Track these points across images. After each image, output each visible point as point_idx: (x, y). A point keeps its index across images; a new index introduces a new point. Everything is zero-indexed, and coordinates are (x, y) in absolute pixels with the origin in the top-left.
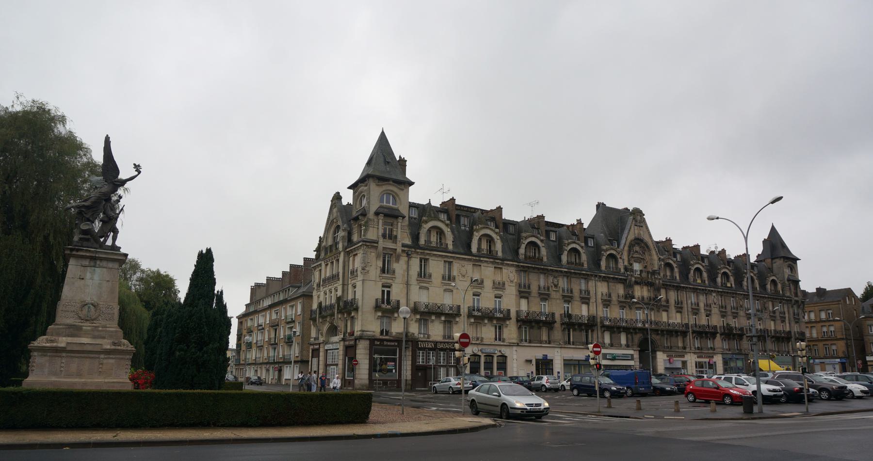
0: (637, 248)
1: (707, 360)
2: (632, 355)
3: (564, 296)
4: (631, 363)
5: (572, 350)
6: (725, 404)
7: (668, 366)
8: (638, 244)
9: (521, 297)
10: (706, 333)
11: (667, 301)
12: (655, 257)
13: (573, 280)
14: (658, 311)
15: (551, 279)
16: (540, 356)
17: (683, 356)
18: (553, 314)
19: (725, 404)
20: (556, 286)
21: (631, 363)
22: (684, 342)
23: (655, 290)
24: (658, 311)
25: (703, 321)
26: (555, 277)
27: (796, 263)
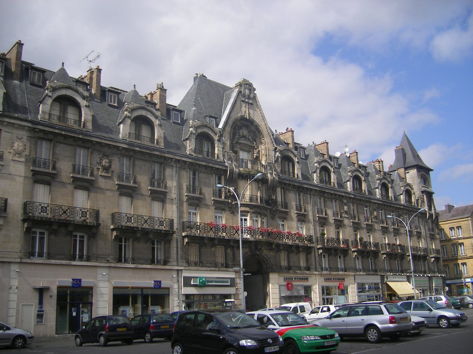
0: (245, 132)
1: (336, 284)
2: (233, 280)
3: (120, 187)
4: (231, 291)
5: (130, 273)
6: (271, 339)
7: (423, 189)
8: (247, 127)
9: (36, 182)
10: (335, 251)
11: (286, 205)
12: (242, 274)
13: (137, 163)
14: (273, 218)
15: (97, 157)
16: (67, 281)
17: (307, 279)
18: (97, 214)
19: (367, 341)
20: (106, 169)
21: (231, 291)
22: (307, 261)
23: (268, 189)
24: (273, 218)
25: (330, 232)
26: (106, 156)
27: (429, 174)
